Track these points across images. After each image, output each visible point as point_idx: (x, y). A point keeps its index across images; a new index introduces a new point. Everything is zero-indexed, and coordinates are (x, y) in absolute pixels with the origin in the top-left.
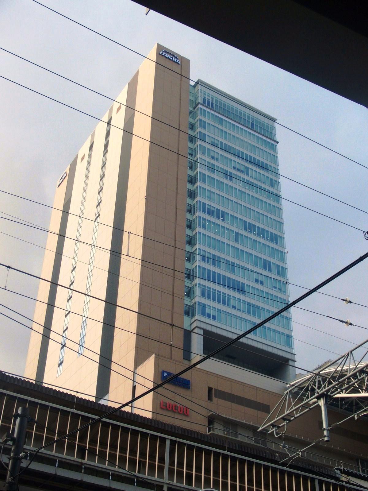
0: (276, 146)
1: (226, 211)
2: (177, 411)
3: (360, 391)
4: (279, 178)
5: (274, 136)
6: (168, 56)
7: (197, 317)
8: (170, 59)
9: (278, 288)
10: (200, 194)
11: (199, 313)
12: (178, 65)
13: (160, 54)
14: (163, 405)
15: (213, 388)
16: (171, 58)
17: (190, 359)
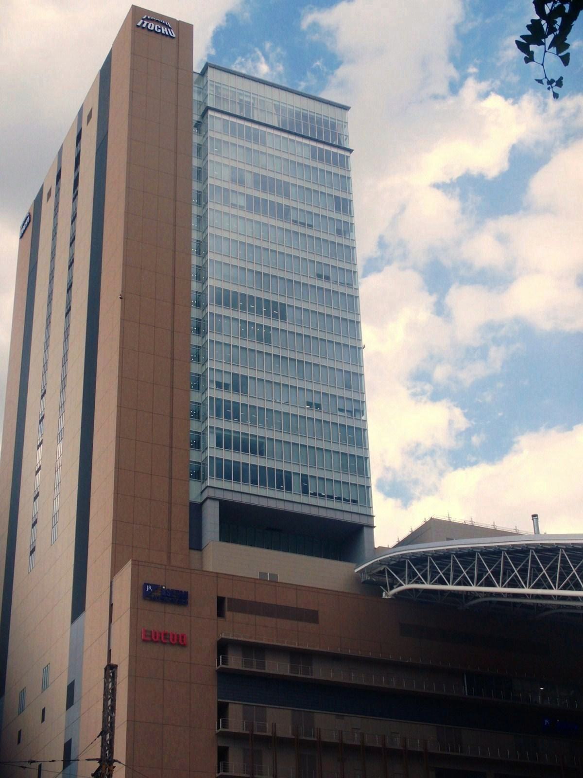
0: (348, 157)
2: (167, 641)
3: (446, 582)
4: (353, 217)
5: (346, 139)
6: (152, 26)
7: (209, 483)
8: (155, 31)
9: (347, 411)
11: (212, 474)
12: (171, 39)
13: (138, 26)
14: (146, 636)
15: (225, 598)
16: (158, 28)
17: (201, 546)
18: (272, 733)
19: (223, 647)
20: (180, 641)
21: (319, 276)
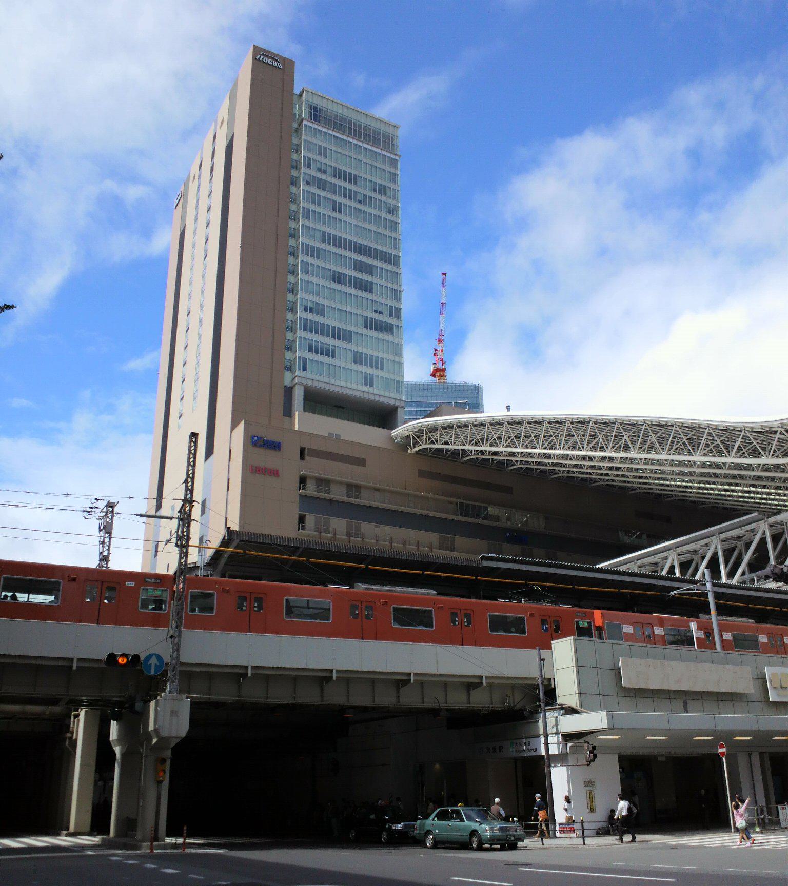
1: (359, 174)
6: (266, 60)
10: (303, 234)
18: (173, 659)
19: (303, 480)
20: (275, 473)
21: (376, 311)
